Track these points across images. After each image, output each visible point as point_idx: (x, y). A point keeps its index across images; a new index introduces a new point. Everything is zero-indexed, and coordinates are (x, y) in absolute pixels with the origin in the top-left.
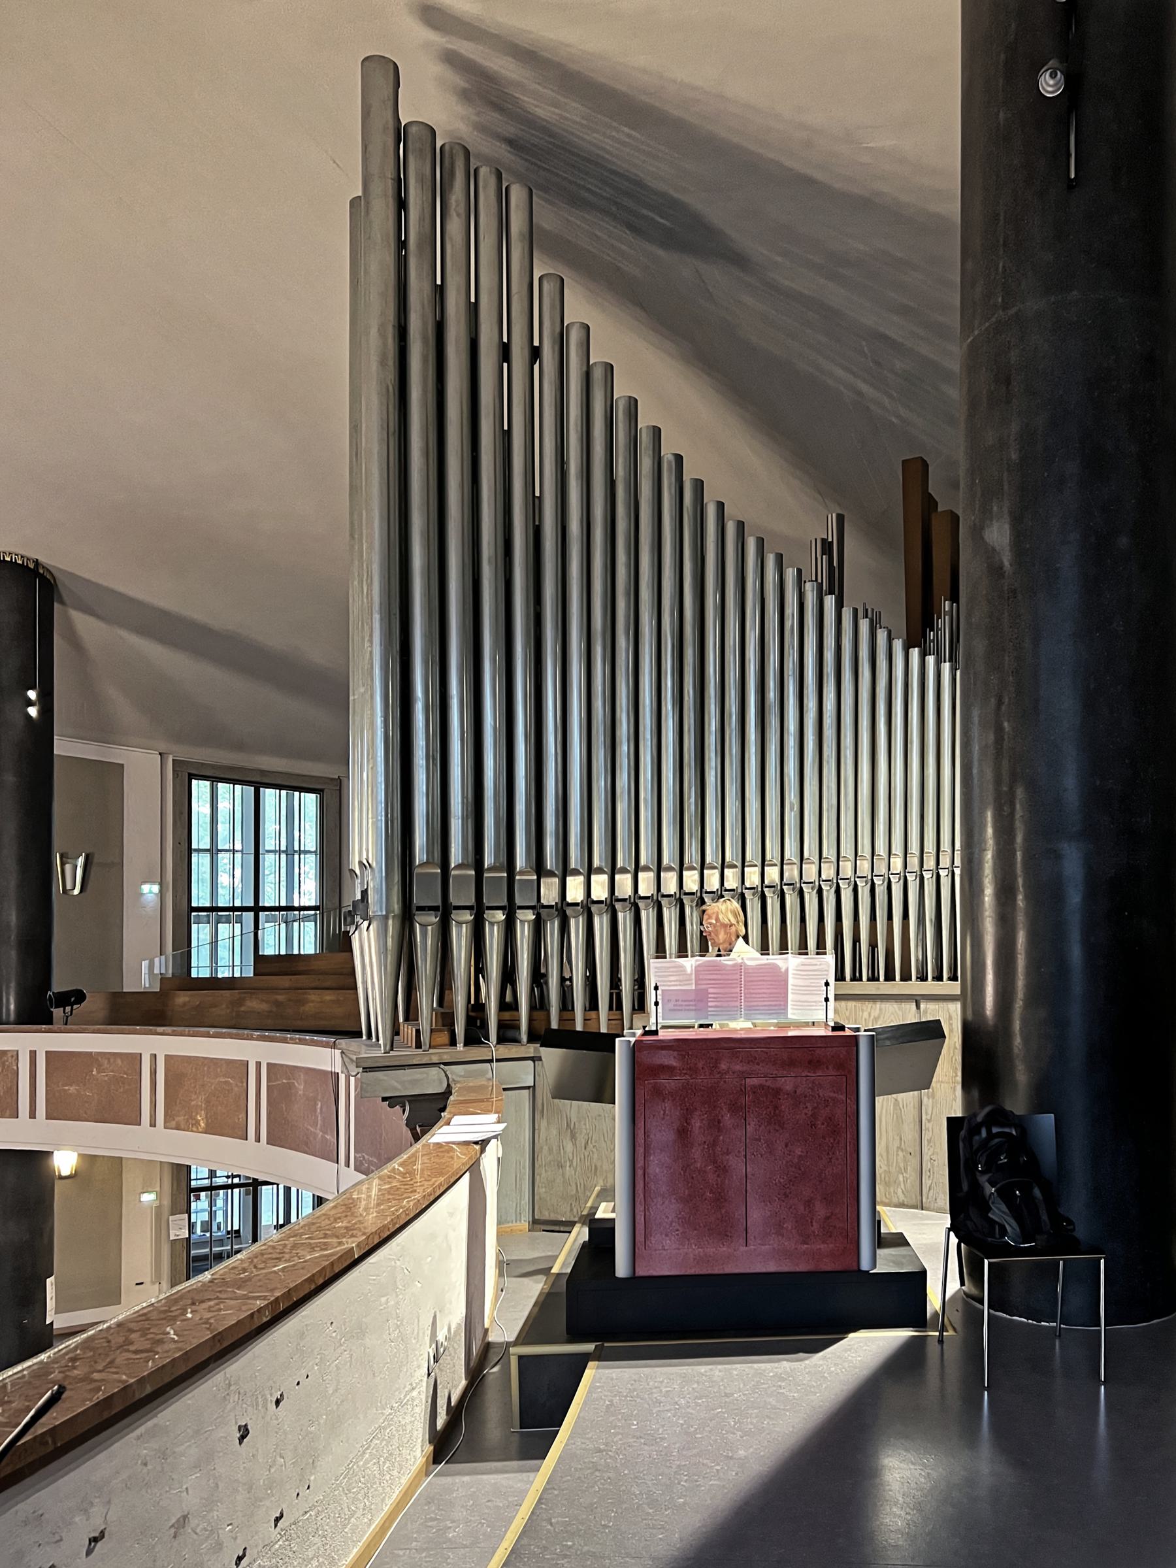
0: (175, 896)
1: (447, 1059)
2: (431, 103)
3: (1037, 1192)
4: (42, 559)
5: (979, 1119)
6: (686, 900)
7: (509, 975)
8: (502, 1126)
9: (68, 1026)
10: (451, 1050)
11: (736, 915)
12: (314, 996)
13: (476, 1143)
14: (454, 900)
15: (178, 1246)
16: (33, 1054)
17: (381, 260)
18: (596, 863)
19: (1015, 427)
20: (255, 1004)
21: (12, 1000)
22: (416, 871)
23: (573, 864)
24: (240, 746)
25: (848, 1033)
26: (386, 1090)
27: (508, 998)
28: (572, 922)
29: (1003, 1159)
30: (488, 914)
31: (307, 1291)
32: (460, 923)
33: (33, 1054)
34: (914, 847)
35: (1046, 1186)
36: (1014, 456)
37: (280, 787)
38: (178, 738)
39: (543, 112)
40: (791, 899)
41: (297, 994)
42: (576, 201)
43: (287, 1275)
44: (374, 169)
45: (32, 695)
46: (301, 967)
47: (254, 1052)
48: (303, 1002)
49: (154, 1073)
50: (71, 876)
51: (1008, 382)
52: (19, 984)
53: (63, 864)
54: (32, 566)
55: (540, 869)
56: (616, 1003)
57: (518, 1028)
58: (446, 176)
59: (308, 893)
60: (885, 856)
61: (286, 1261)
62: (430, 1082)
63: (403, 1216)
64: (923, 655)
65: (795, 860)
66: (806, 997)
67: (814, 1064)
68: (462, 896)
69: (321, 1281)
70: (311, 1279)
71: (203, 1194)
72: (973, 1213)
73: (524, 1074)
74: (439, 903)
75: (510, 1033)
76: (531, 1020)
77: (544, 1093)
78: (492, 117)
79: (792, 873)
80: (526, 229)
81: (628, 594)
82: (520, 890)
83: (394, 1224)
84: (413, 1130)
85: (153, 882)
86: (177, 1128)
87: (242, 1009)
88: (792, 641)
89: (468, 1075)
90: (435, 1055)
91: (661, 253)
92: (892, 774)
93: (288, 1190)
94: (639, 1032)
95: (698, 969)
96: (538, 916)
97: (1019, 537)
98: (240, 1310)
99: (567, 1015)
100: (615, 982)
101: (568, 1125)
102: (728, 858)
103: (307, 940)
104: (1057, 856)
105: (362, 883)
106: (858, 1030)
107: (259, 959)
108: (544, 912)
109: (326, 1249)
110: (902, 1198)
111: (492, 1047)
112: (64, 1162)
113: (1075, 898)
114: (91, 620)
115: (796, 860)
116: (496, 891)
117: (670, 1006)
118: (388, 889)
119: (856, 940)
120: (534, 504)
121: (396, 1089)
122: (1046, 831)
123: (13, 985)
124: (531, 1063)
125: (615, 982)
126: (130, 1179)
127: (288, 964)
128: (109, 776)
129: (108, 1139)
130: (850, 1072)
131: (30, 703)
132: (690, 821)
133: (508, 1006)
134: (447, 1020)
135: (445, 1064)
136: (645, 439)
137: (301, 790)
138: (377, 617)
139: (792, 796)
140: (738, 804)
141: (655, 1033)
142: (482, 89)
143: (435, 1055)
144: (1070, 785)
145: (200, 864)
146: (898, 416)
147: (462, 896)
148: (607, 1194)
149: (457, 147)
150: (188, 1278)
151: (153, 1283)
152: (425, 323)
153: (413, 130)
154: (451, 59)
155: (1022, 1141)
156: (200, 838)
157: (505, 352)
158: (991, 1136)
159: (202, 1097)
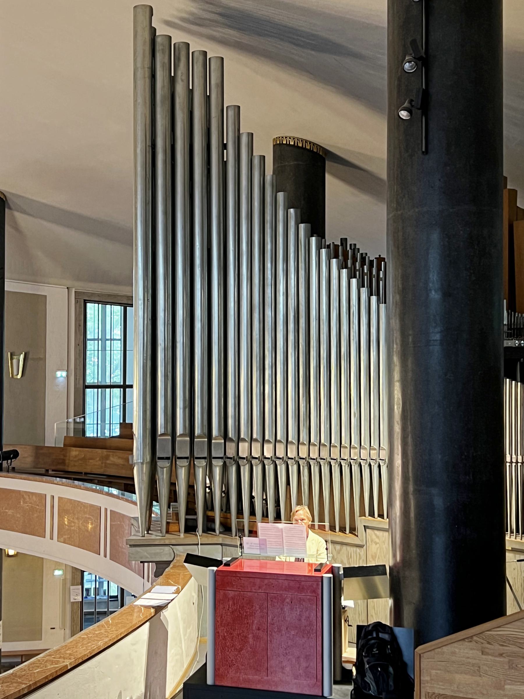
1: (174, 542)
13: (153, 607)
15: (75, 606)
26: (141, 558)
31: (44, 682)
38: (78, 278)
43: (52, 668)
44: (139, 65)
49: (52, 507)
53: (12, 359)
58: (177, 61)
61: (41, 668)
63: (97, 649)
65: (356, 446)
67: (301, 589)
68: (183, 451)
69: (51, 678)
70: (46, 677)
80: (219, 81)
82: (214, 448)
83: (91, 654)
86: (64, 542)
87: (108, 462)
96: (225, 463)
98: (16, 688)
109: (57, 664)
118: (144, 448)
121: (147, 557)
124: (220, 546)
128: (37, 303)
130: (318, 595)
135: (173, 545)
147: (183, 451)
149: (182, 44)
150: (81, 630)
151: (61, 629)
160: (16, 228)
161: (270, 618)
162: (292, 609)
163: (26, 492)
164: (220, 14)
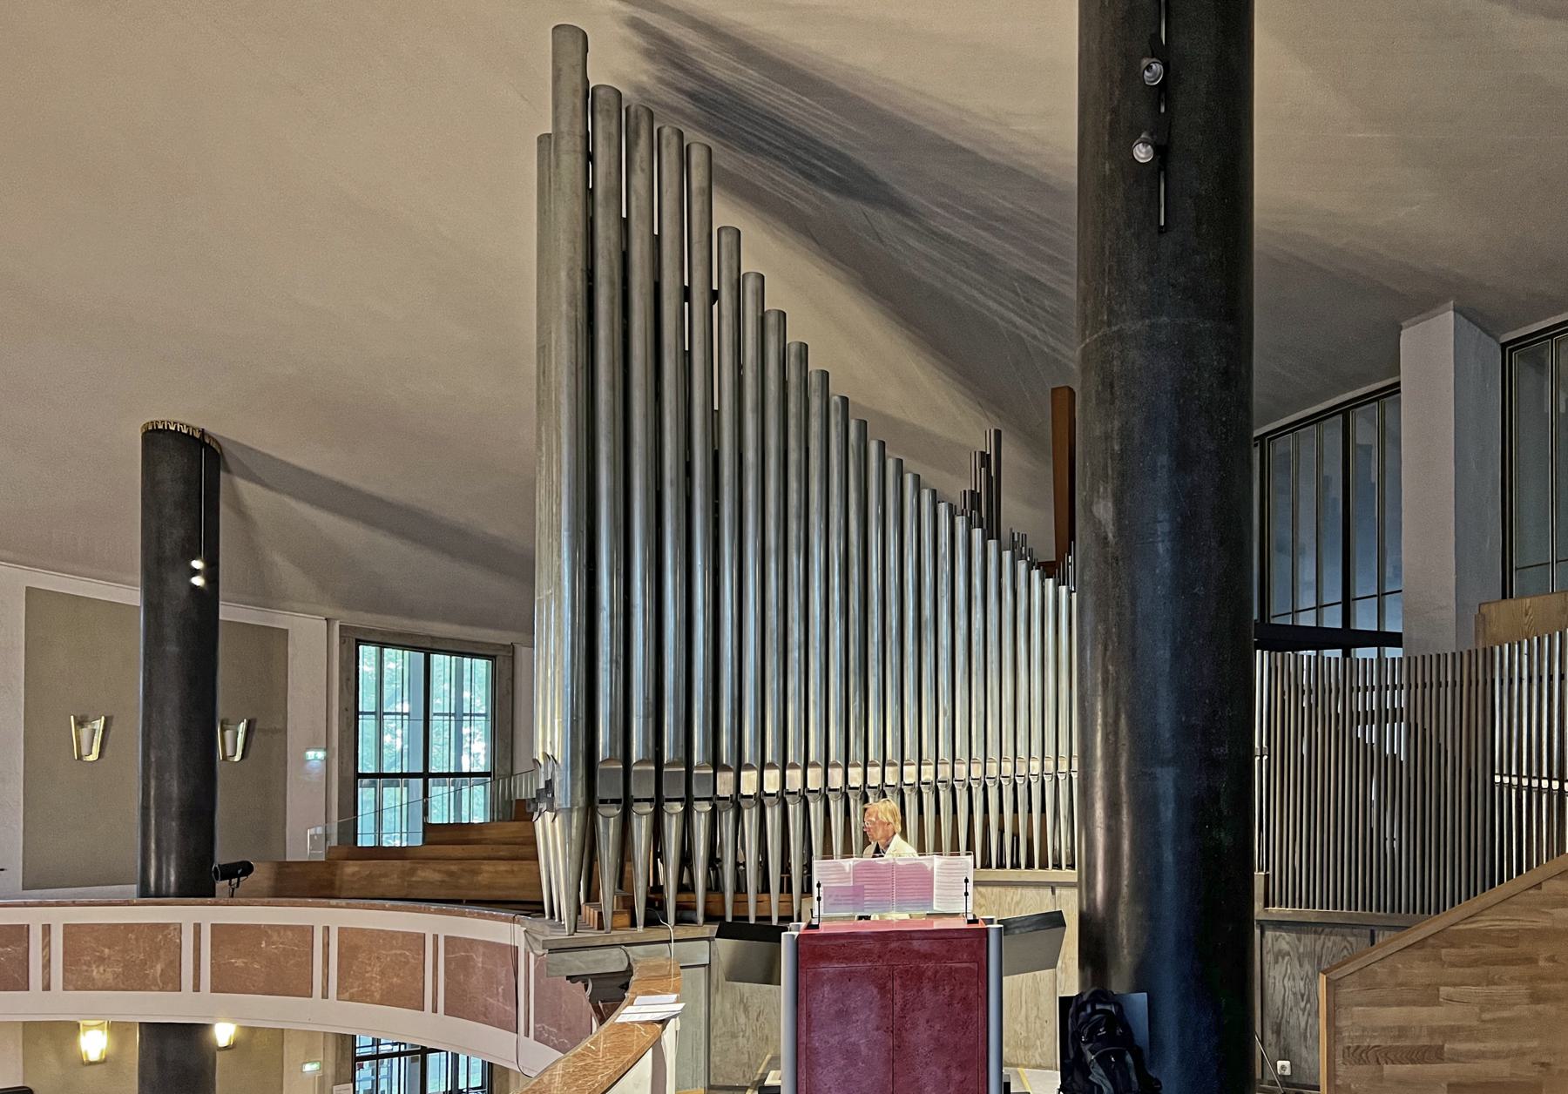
0: (341, 763)
1: (628, 940)
2: (616, 64)
3: (1129, 1058)
4: (208, 429)
5: (1085, 998)
6: (851, 794)
7: (686, 859)
8: (680, 1006)
9: (233, 897)
10: (631, 931)
11: (893, 815)
12: (488, 867)
14: (635, 793)
16: (197, 927)
17: (568, 211)
18: (769, 758)
19: (1117, 424)
20: (429, 874)
21: (172, 872)
22: (600, 767)
23: (747, 760)
24: (411, 613)
25: (981, 925)
27: (685, 880)
28: (746, 812)
29: (1102, 1031)
30: (667, 806)
32: (640, 815)
33: (197, 927)
34: (1050, 752)
35: (1137, 1053)
36: (1117, 448)
37: (450, 653)
38: (348, 604)
39: (722, 74)
40: (944, 795)
41: (472, 865)
42: (749, 147)
45: (197, 564)
46: (474, 836)
47: (434, 925)
48: (475, 872)
49: (326, 945)
50: (232, 742)
51: (1112, 386)
52: (180, 857)
53: (223, 730)
54: (197, 435)
55: (716, 764)
56: (786, 887)
57: (695, 910)
58: (632, 135)
59: (477, 755)
60: (1026, 758)
62: (612, 961)
64: (1057, 586)
66: (953, 892)
68: (643, 788)
71: (366, 1063)
72: (1077, 1076)
73: (700, 953)
74: (620, 795)
75: (687, 914)
76: (707, 902)
77: (719, 973)
78: (672, 74)
79: (945, 771)
81: (799, 517)
84: (596, 1009)
85: (318, 749)
88: (944, 566)
89: (648, 955)
90: (618, 936)
91: (832, 197)
92: (1032, 685)
93: (456, 1057)
94: (803, 924)
95: (856, 869)
96: (714, 808)
97: (1120, 513)
99: (740, 897)
100: (785, 868)
101: (741, 1000)
102: (889, 757)
103: (476, 807)
104: (1153, 777)
105: (546, 773)
106: (991, 921)
107: (428, 827)
108: (720, 804)
110: (1039, 1060)
111: (671, 929)
112: (224, 1033)
113: (1168, 813)
114: (252, 486)
115: (949, 760)
116: (673, 784)
117: (831, 900)
118: (573, 785)
119: (1001, 831)
120: (713, 417)
121: (579, 968)
122: (1145, 756)
123: (173, 856)
125: (785, 868)
126: (291, 1051)
127: (457, 833)
129: (270, 1010)
131: (195, 572)
132: (853, 719)
133: (685, 888)
134: (628, 904)
136: (814, 381)
137: (473, 656)
138: (565, 534)
139: (944, 702)
140: (898, 708)
141: (817, 927)
142: (664, 51)
143: (618, 936)
144: (1165, 719)
145: (367, 726)
146: (1048, 346)
147: (643, 788)
148: (774, 1063)
152: (611, 268)
153: (600, 93)
154: (636, 25)
155: (1118, 1019)
156: (367, 702)
157: (686, 294)
158: (1094, 1012)
159: (377, 969)
160: (240, 510)
161: (897, 1008)
162: (935, 988)
163: (270, 926)
164: (693, 96)
